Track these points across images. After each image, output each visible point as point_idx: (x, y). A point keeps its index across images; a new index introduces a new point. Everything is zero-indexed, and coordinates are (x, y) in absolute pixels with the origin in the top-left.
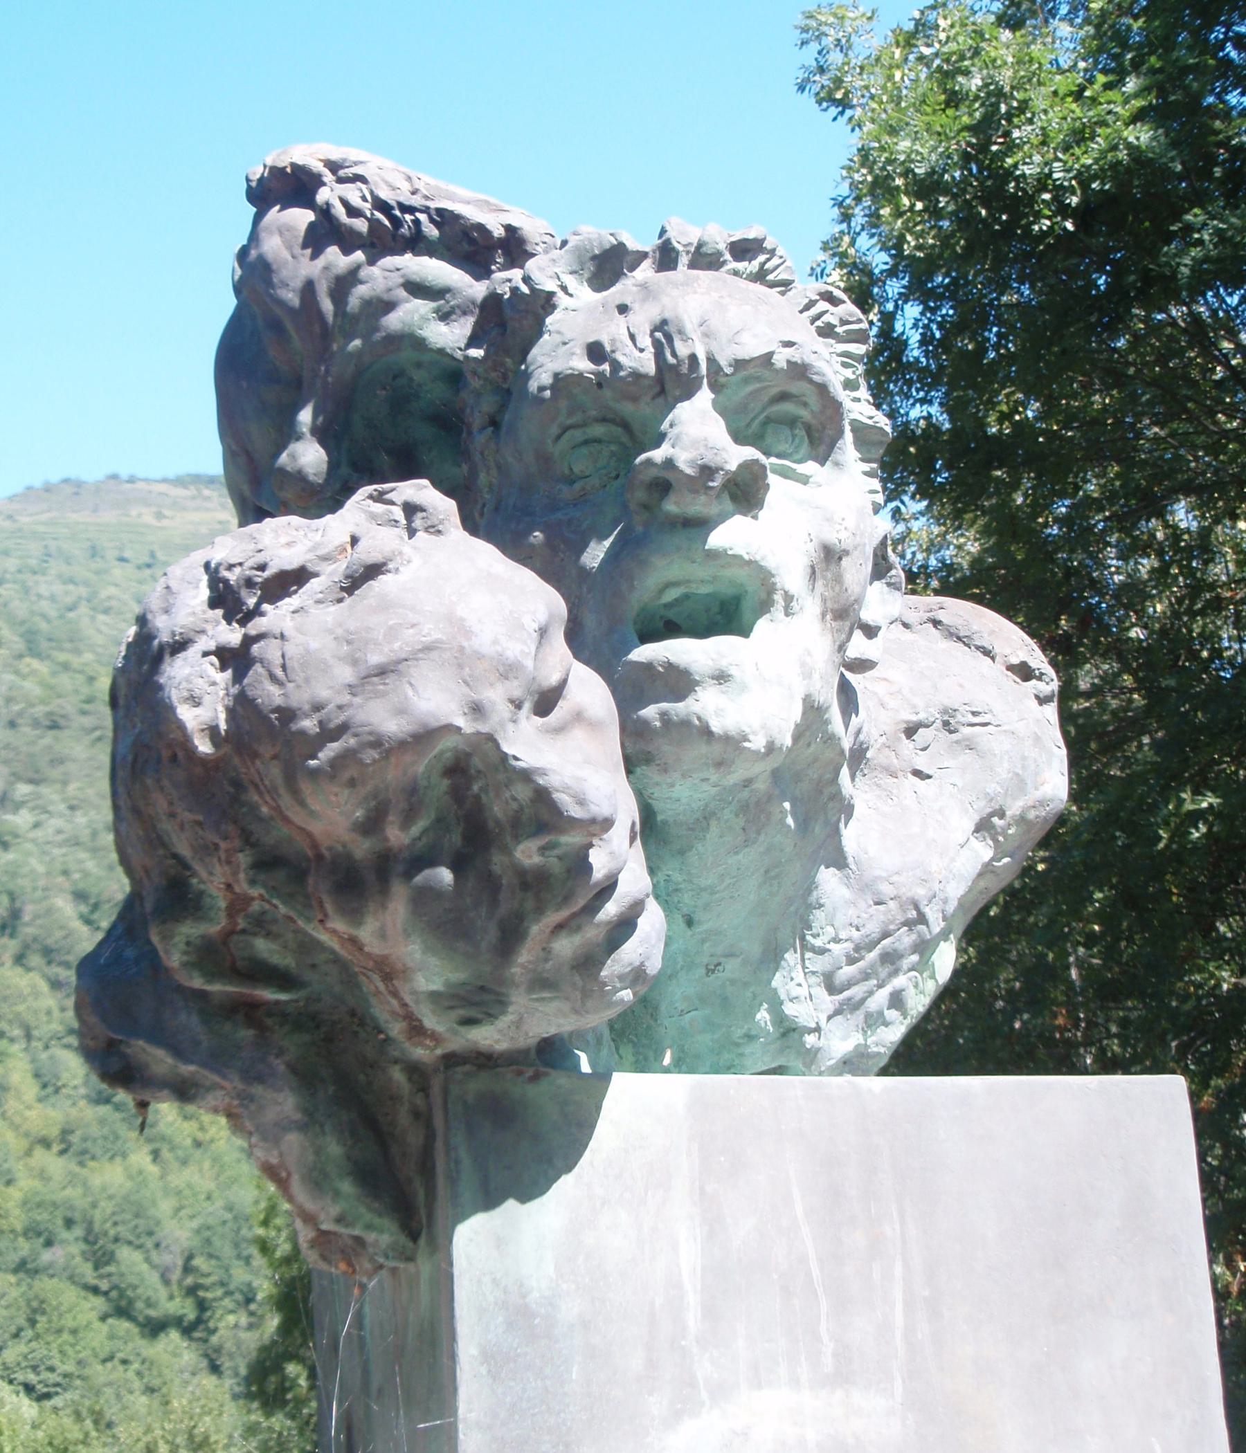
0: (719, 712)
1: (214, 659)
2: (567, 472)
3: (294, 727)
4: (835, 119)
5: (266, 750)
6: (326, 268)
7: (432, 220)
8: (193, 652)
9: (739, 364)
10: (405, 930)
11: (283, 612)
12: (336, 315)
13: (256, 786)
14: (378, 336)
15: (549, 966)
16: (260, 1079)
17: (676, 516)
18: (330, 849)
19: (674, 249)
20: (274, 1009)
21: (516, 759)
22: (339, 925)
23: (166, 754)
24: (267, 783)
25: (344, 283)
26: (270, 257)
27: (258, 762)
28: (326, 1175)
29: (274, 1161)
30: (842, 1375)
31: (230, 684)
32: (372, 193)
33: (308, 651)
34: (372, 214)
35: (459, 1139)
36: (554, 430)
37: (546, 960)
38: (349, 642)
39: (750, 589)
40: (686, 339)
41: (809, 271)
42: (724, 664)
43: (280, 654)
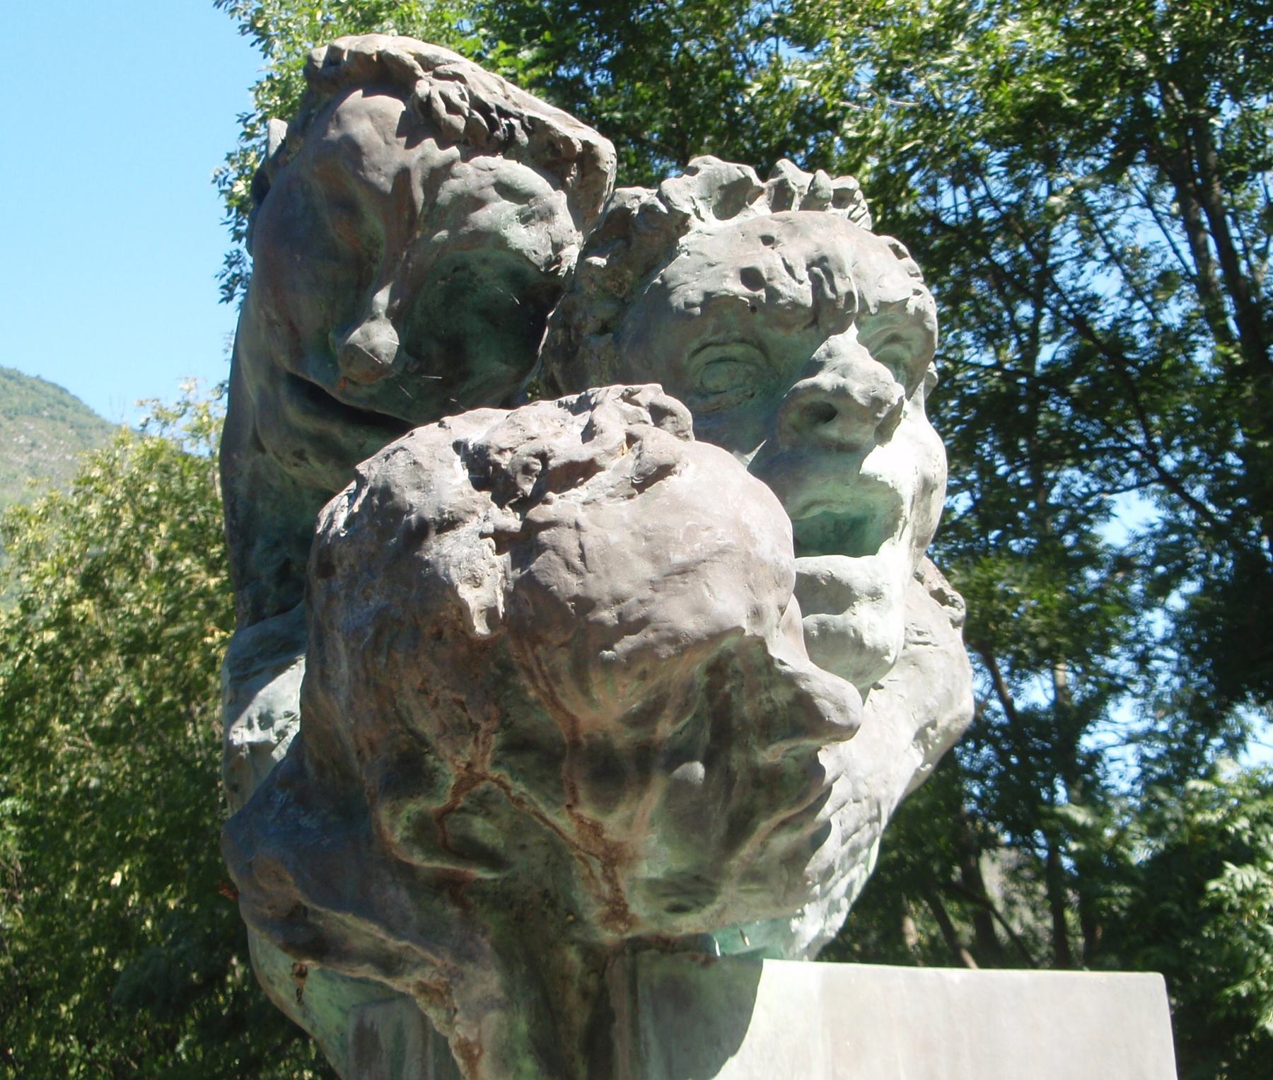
0: (871, 627)
1: (491, 540)
2: (697, 385)
3: (592, 617)
4: (253, 45)
5: (556, 637)
6: (423, 159)
7: (524, 127)
8: (462, 531)
9: (883, 305)
10: (652, 820)
11: (572, 502)
12: (424, 204)
13: (529, 671)
14: (465, 230)
15: (761, 860)
16: (471, 957)
17: (833, 441)
18: (589, 736)
19: (790, 189)
20: (477, 887)
21: (782, 663)
22: (587, 812)
23: (428, 630)
24: (545, 668)
26: (361, 140)
27: (540, 648)
28: (513, 1053)
29: (471, 1038)
31: (509, 566)
32: (470, 93)
33: (607, 543)
34: (471, 113)
35: (646, 1021)
36: (695, 345)
37: (761, 854)
38: (647, 539)
39: (879, 513)
40: (844, 277)
41: (212, 178)
42: (879, 582)
43: (576, 543)
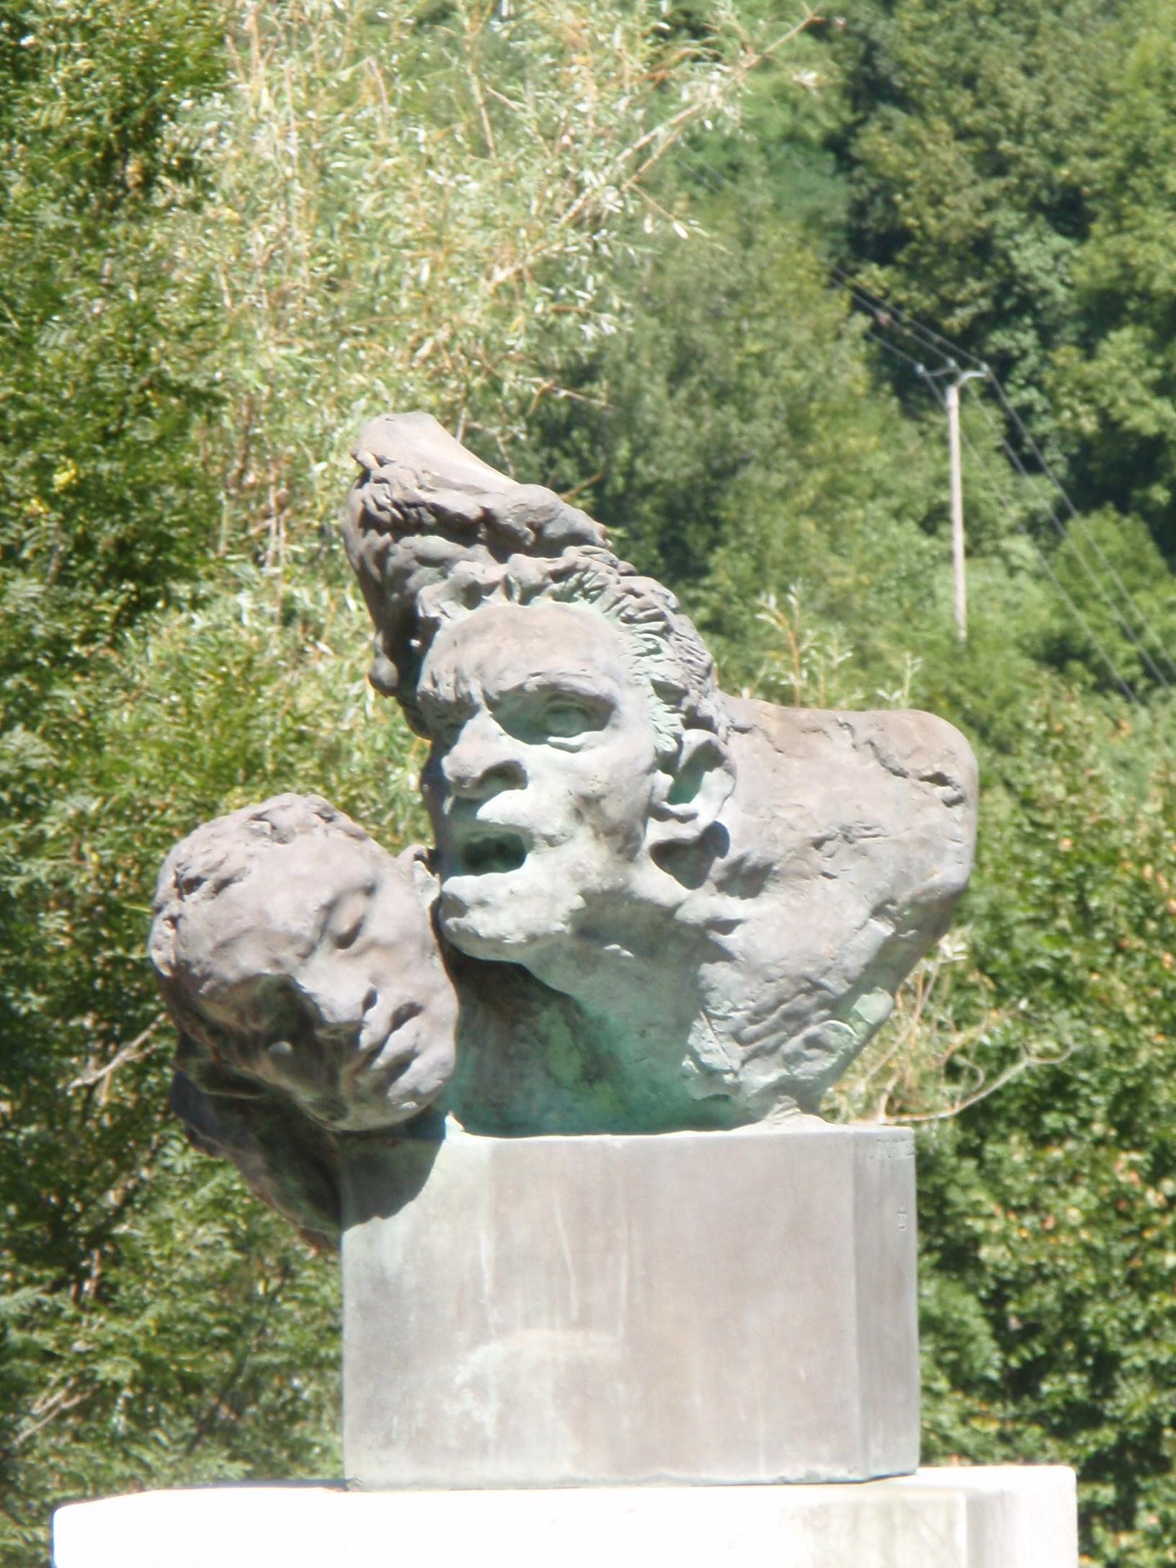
25: (382, 556)
30: (584, 1321)
42: (482, 895)
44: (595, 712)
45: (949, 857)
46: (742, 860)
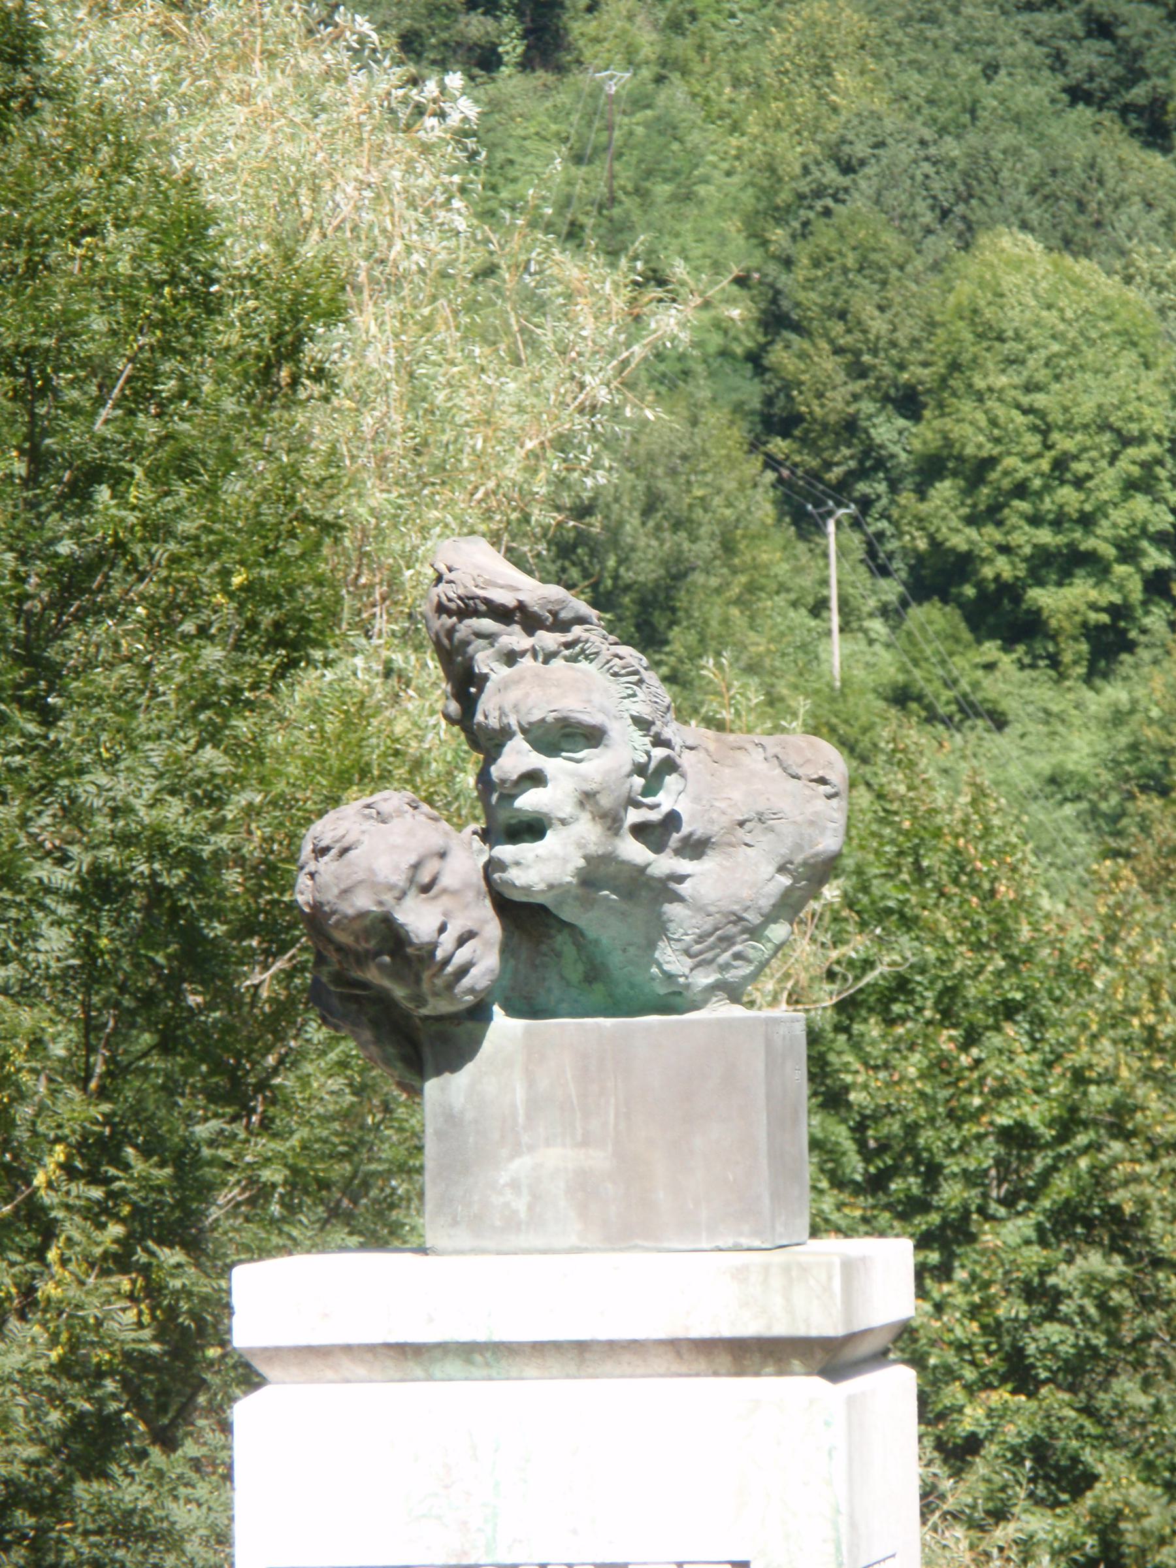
25: (451, 632)
30: (585, 1143)
44: (593, 736)
45: (829, 833)
46: (691, 835)
